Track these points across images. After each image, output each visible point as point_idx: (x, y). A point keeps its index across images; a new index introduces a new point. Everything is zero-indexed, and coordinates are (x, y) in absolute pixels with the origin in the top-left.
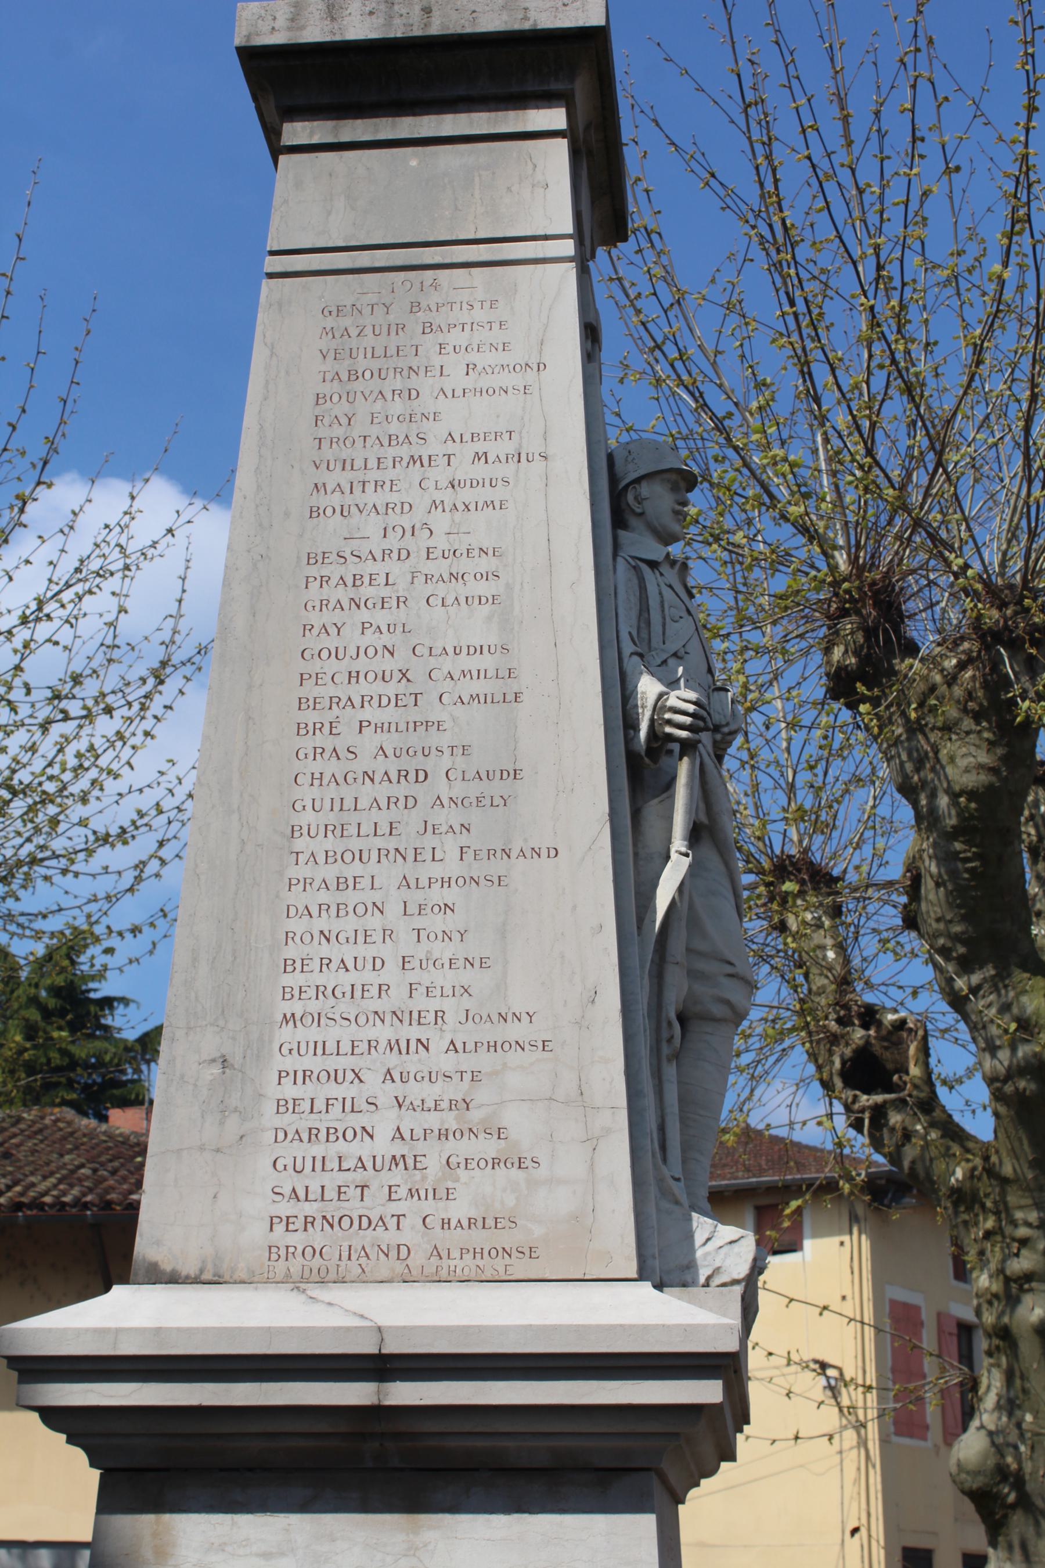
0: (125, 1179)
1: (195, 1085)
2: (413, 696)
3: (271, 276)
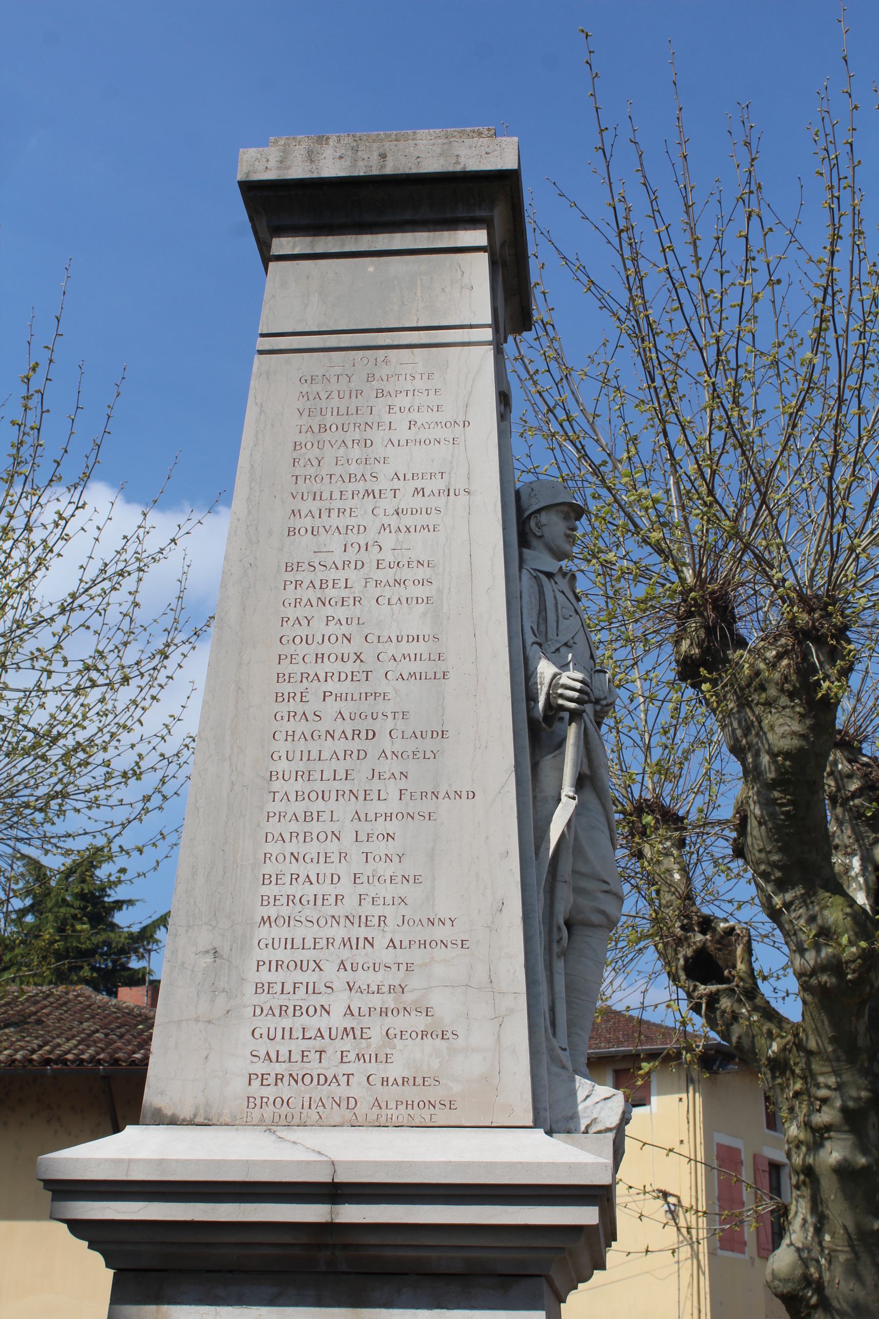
0: (129, 1042)
1: (193, 971)
2: (365, 674)
3: (261, 352)
